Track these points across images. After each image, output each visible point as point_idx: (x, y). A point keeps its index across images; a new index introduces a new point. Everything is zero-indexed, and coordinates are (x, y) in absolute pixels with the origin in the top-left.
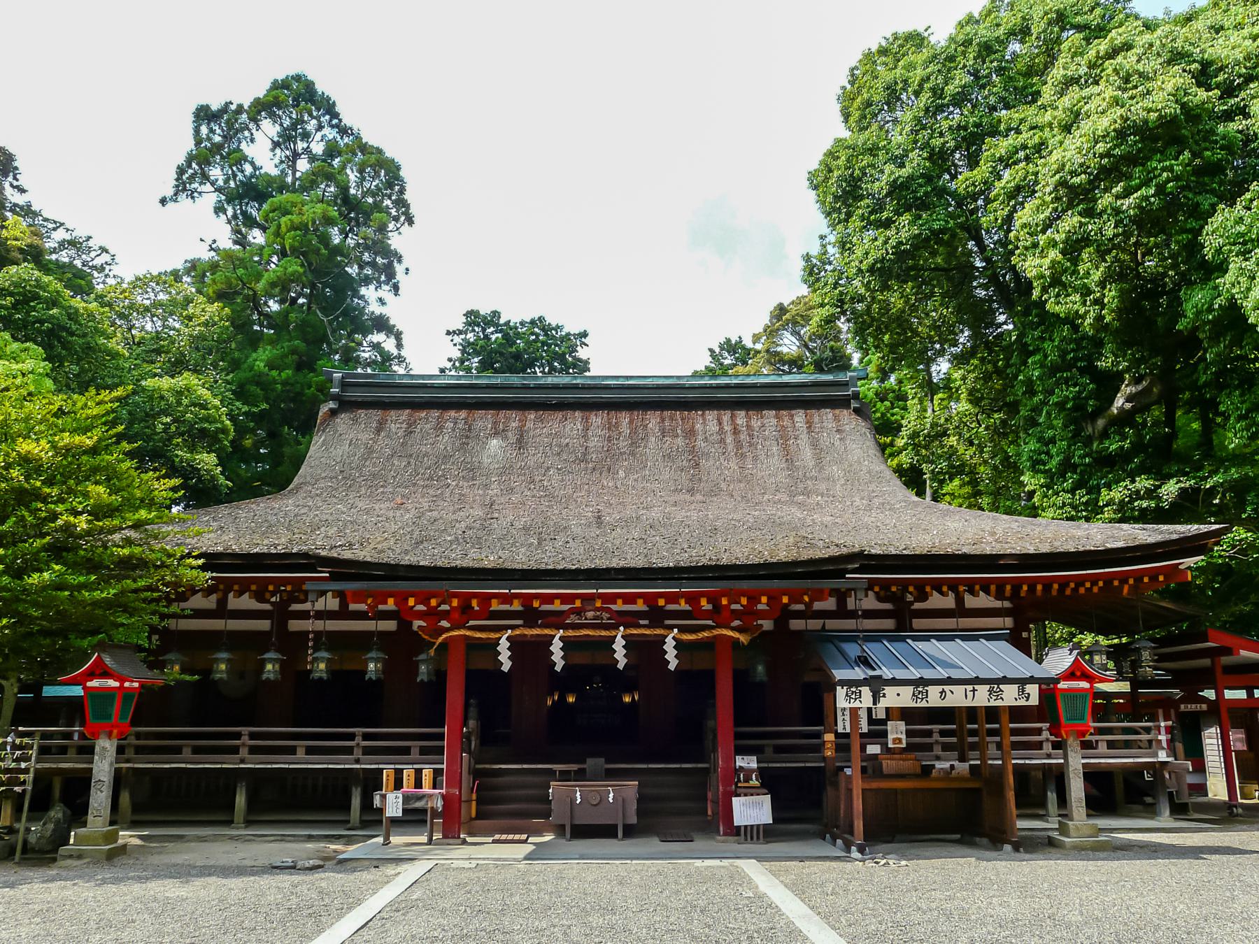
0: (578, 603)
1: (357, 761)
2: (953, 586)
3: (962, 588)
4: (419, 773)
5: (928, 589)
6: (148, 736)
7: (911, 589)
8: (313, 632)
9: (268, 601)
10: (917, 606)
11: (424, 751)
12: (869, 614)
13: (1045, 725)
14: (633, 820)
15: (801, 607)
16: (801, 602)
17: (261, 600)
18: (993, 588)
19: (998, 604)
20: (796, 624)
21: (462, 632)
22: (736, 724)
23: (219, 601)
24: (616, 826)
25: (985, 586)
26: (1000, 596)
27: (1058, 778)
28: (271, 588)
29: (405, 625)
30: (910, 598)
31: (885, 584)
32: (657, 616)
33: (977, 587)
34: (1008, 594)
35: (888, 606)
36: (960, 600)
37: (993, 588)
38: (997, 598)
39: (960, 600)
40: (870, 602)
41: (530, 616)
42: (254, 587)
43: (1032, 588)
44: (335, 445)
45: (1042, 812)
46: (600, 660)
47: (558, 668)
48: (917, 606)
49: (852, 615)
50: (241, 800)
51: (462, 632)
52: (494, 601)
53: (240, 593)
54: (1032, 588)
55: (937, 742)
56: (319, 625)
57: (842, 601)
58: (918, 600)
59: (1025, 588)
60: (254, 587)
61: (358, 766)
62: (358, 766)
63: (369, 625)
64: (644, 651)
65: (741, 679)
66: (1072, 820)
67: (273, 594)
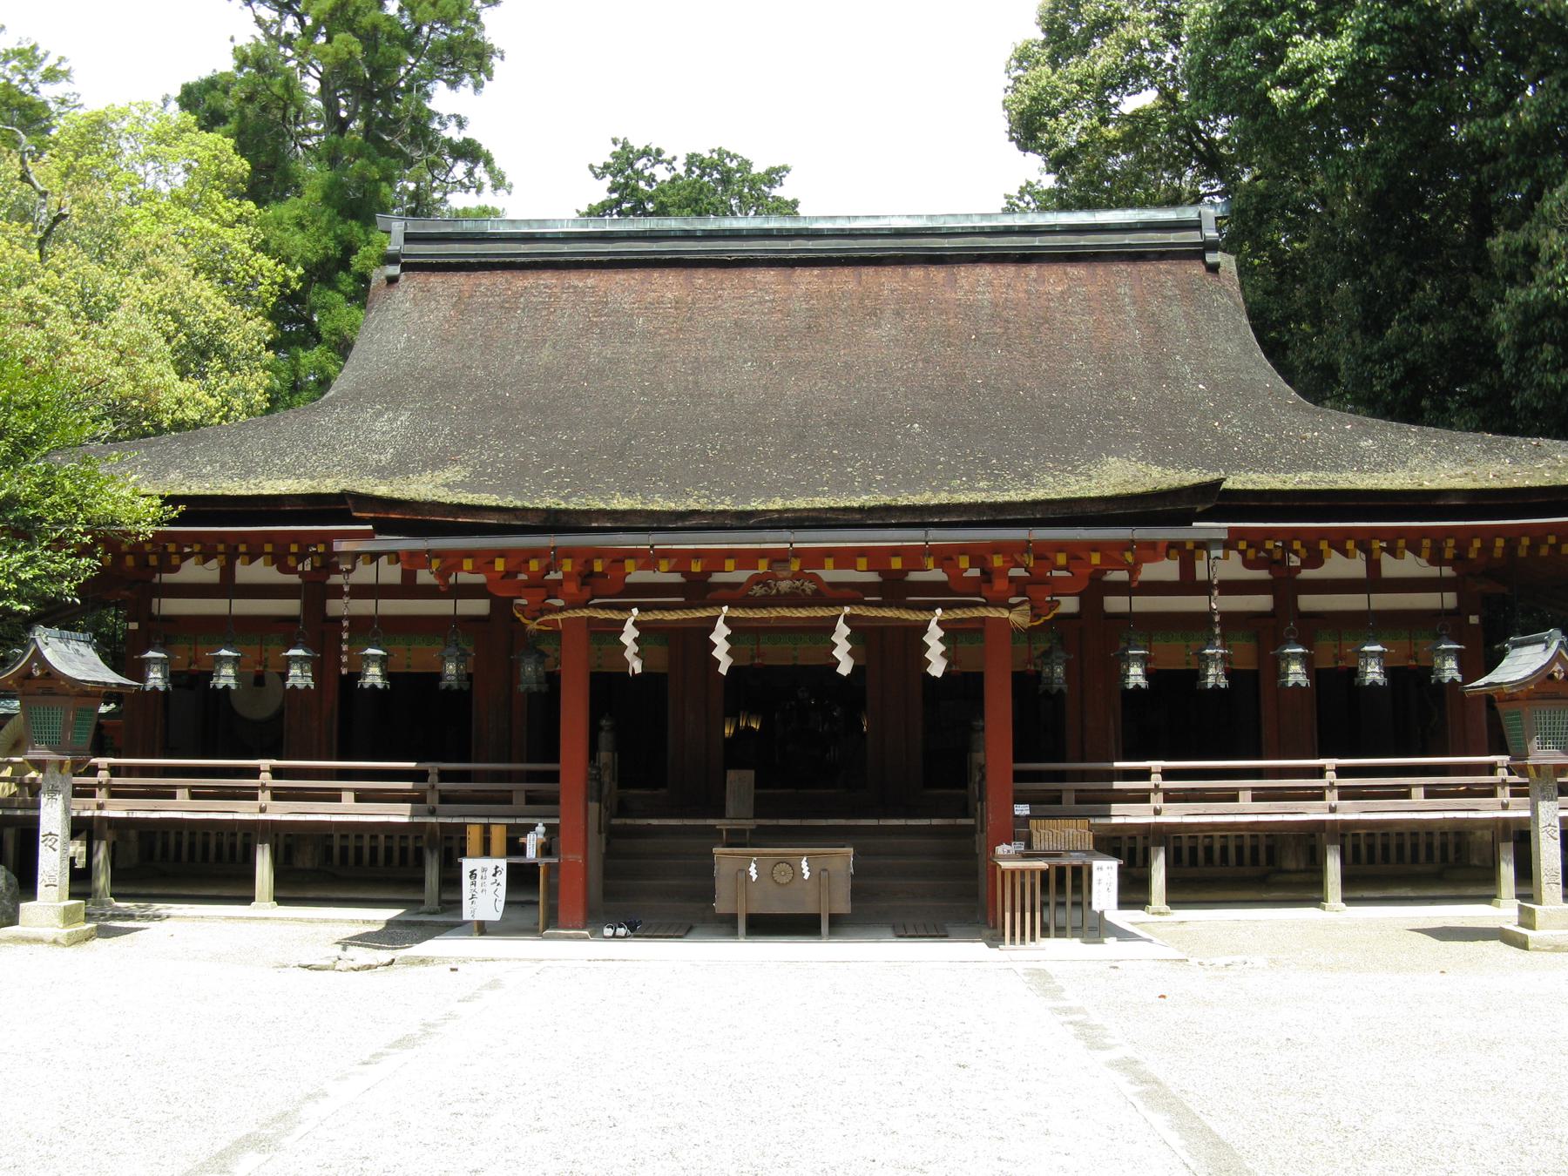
0: (763, 566)
1: (1505, 807)
2: (1364, 542)
3: (1377, 544)
4: (486, 829)
5: (1324, 545)
6: (130, 771)
7: (1297, 545)
8: (349, 618)
9: (293, 571)
10: (1306, 574)
11: (531, 800)
12: (1229, 587)
13: (1502, 759)
14: (843, 906)
15: (1121, 576)
16: (1122, 565)
17: (284, 569)
18: (1426, 543)
19: (1433, 571)
20: (1115, 604)
21: (586, 613)
22: (1016, 759)
23: (223, 570)
24: (817, 917)
25: (1413, 543)
26: (1436, 559)
27: (1522, 838)
28: (294, 548)
29: (502, 606)
30: (1295, 561)
31: (1256, 540)
32: (698, 590)
33: (1401, 543)
34: (1449, 554)
35: (1263, 574)
36: (1373, 565)
37: (1426, 543)
38: (1432, 562)
39: (1373, 565)
40: (1231, 567)
41: (894, 589)
42: (268, 548)
43: (1462, 548)
44: (404, 324)
45: (1316, 896)
46: (802, 653)
47: (723, 670)
48: (1306, 574)
49: (1205, 588)
50: (1333, 866)
51: (586, 613)
52: (629, 565)
53: (252, 558)
54: (1512, 545)
55: (264, 787)
56: (364, 607)
57: (1187, 567)
58: (1306, 564)
59: (1477, 543)
60: (268, 548)
61: (433, 820)
62: (433, 820)
63: (442, 607)
64: (890, 648)
65: (1026, 686)
66: (1539, 903)
67: (301, 558)
